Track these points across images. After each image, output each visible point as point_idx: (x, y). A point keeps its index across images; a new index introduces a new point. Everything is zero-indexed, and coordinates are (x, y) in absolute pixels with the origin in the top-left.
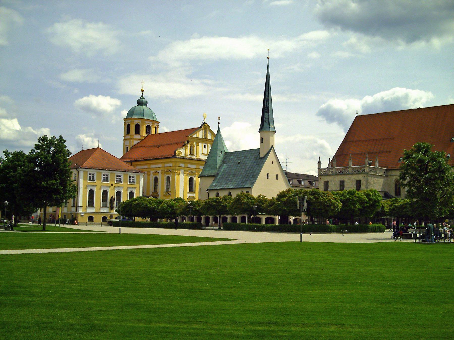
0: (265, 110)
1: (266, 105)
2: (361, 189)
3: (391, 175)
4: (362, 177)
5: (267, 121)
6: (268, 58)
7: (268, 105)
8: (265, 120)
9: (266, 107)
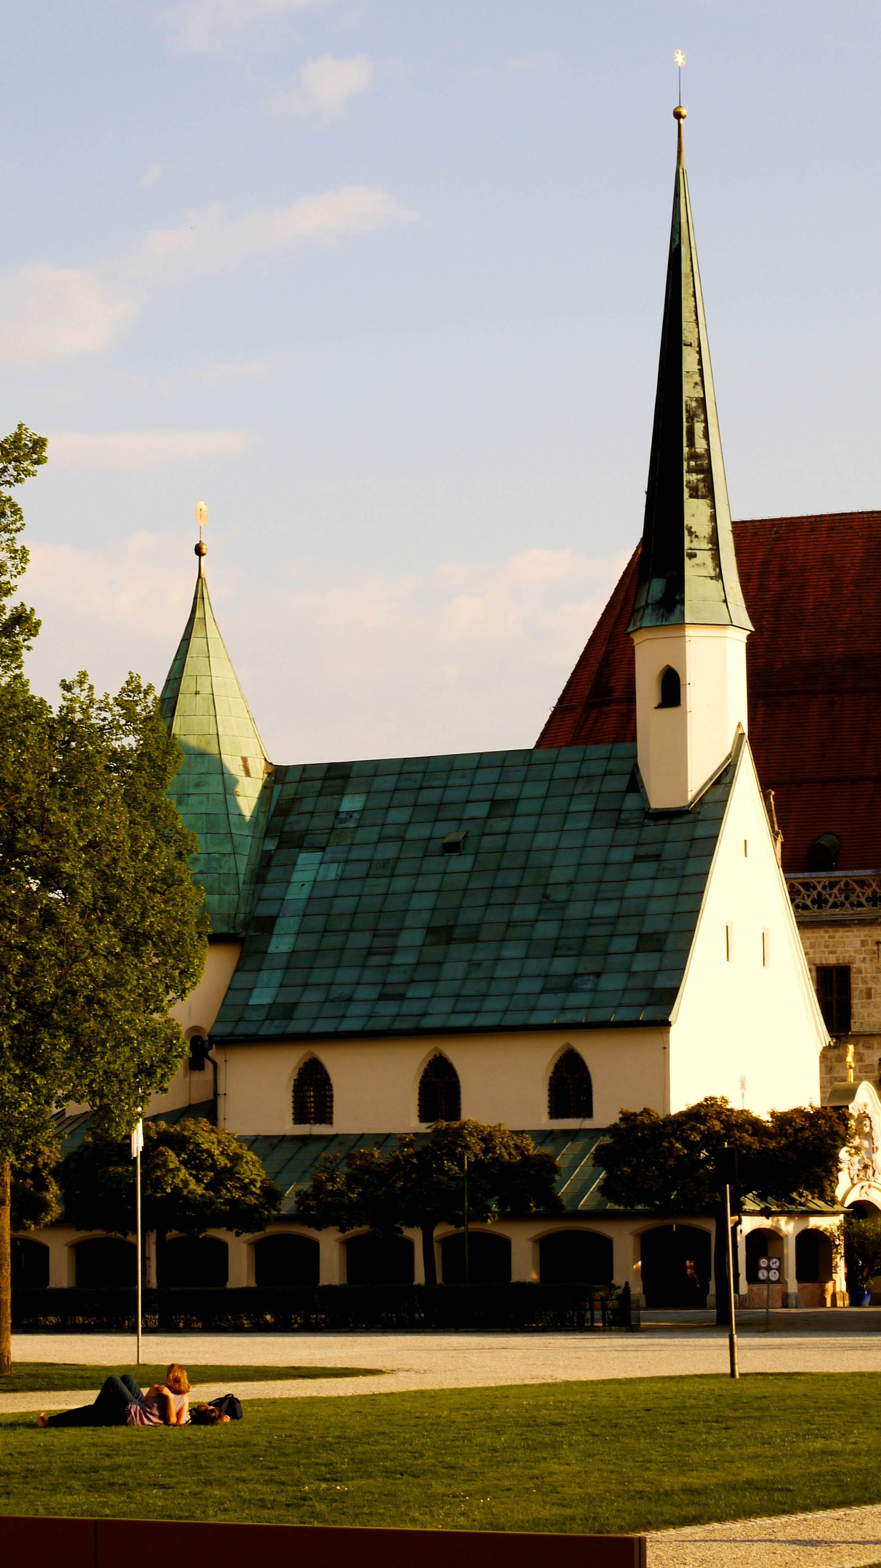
0: (687, 477)
1: (691, 444)
2: (855, 1028)
3: (237, 869)
4: (863, 943)
5: (705, 557)
6: (678, 116)
7: (700, 445)
8: (687, 545)
9: (694, 456)
